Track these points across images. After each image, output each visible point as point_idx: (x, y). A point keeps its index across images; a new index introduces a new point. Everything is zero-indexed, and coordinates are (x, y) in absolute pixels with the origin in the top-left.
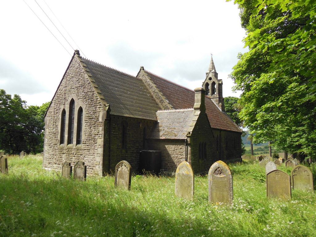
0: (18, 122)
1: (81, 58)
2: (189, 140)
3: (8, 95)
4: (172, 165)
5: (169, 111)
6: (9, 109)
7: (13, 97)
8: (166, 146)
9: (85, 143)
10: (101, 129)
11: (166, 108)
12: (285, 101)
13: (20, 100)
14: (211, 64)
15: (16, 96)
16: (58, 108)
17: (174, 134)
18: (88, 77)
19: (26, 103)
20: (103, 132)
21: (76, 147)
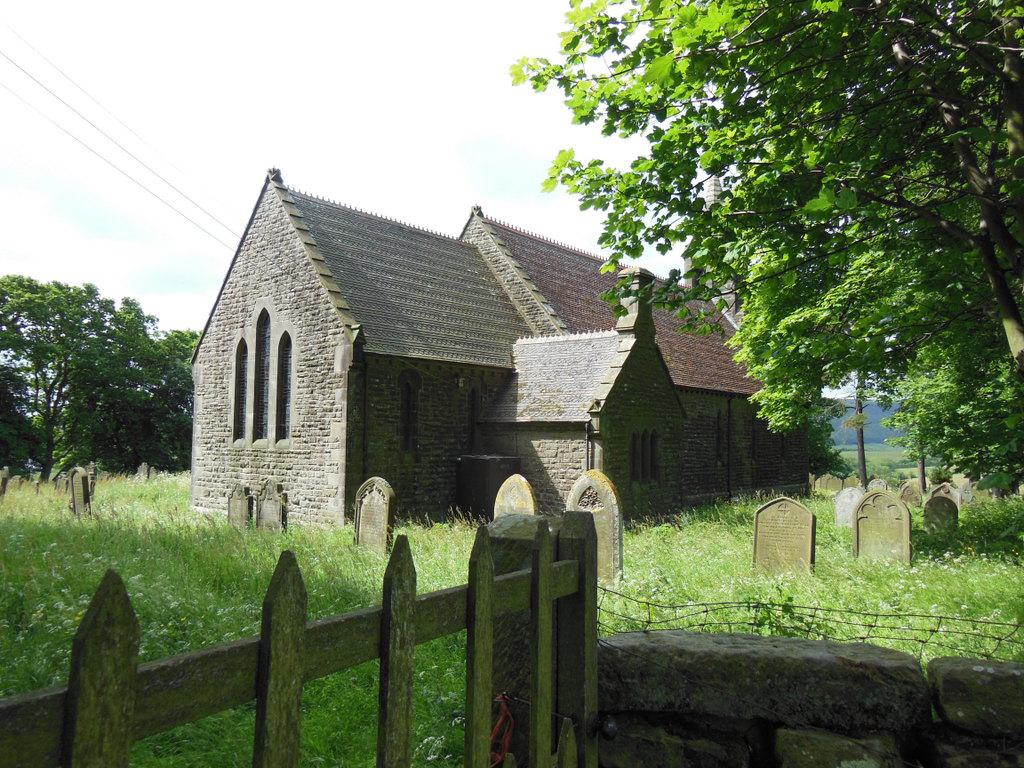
0: (137, 378)
1: (283, 190)
2: (595, 423)
3: (106, 301)
4: (550, 498)
5: (556, 338)
6: (109, 340)
7: (118, 306)
8: (535, 443)
9: (299, 436)
10: (339, 395)
11: (546, 331)
12: (838, 305)
13: (139, 312)
14: (713, 188)
15: (126, 302)
16: (226, 338)
17: (557, 406)
18: (303, 247)
19: (157, 324)
20: (346, 403)
21: (275, 447)
